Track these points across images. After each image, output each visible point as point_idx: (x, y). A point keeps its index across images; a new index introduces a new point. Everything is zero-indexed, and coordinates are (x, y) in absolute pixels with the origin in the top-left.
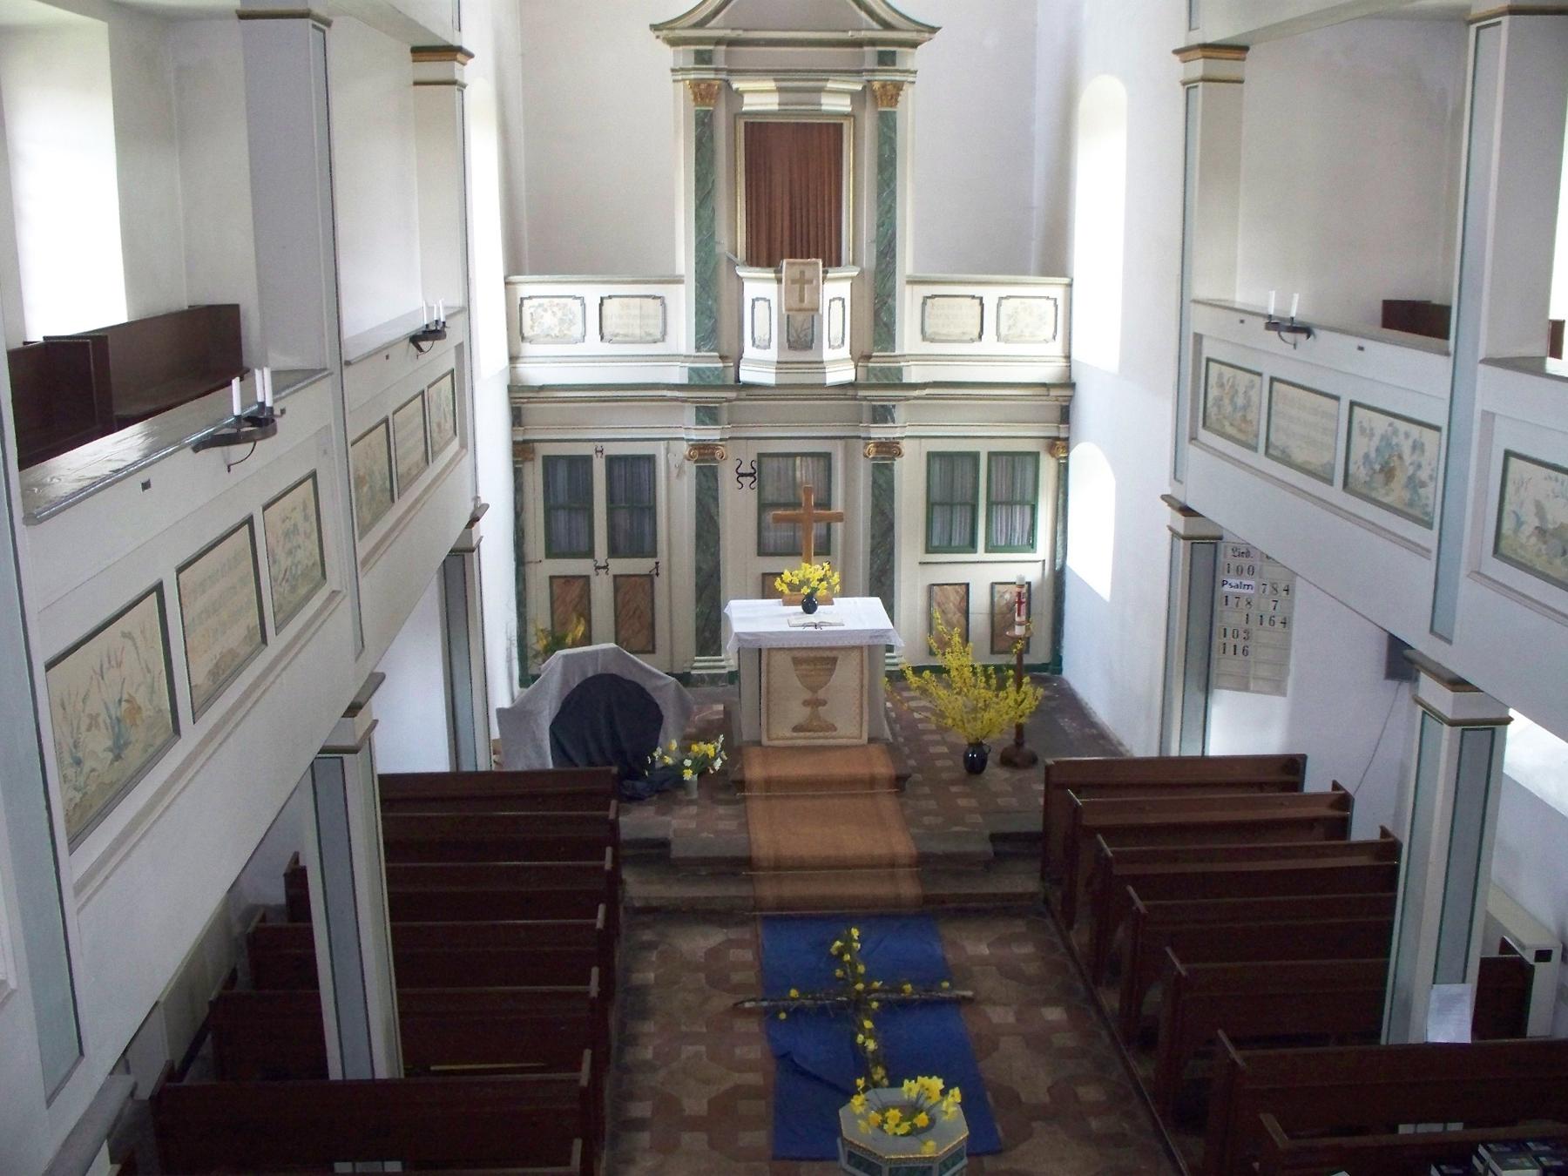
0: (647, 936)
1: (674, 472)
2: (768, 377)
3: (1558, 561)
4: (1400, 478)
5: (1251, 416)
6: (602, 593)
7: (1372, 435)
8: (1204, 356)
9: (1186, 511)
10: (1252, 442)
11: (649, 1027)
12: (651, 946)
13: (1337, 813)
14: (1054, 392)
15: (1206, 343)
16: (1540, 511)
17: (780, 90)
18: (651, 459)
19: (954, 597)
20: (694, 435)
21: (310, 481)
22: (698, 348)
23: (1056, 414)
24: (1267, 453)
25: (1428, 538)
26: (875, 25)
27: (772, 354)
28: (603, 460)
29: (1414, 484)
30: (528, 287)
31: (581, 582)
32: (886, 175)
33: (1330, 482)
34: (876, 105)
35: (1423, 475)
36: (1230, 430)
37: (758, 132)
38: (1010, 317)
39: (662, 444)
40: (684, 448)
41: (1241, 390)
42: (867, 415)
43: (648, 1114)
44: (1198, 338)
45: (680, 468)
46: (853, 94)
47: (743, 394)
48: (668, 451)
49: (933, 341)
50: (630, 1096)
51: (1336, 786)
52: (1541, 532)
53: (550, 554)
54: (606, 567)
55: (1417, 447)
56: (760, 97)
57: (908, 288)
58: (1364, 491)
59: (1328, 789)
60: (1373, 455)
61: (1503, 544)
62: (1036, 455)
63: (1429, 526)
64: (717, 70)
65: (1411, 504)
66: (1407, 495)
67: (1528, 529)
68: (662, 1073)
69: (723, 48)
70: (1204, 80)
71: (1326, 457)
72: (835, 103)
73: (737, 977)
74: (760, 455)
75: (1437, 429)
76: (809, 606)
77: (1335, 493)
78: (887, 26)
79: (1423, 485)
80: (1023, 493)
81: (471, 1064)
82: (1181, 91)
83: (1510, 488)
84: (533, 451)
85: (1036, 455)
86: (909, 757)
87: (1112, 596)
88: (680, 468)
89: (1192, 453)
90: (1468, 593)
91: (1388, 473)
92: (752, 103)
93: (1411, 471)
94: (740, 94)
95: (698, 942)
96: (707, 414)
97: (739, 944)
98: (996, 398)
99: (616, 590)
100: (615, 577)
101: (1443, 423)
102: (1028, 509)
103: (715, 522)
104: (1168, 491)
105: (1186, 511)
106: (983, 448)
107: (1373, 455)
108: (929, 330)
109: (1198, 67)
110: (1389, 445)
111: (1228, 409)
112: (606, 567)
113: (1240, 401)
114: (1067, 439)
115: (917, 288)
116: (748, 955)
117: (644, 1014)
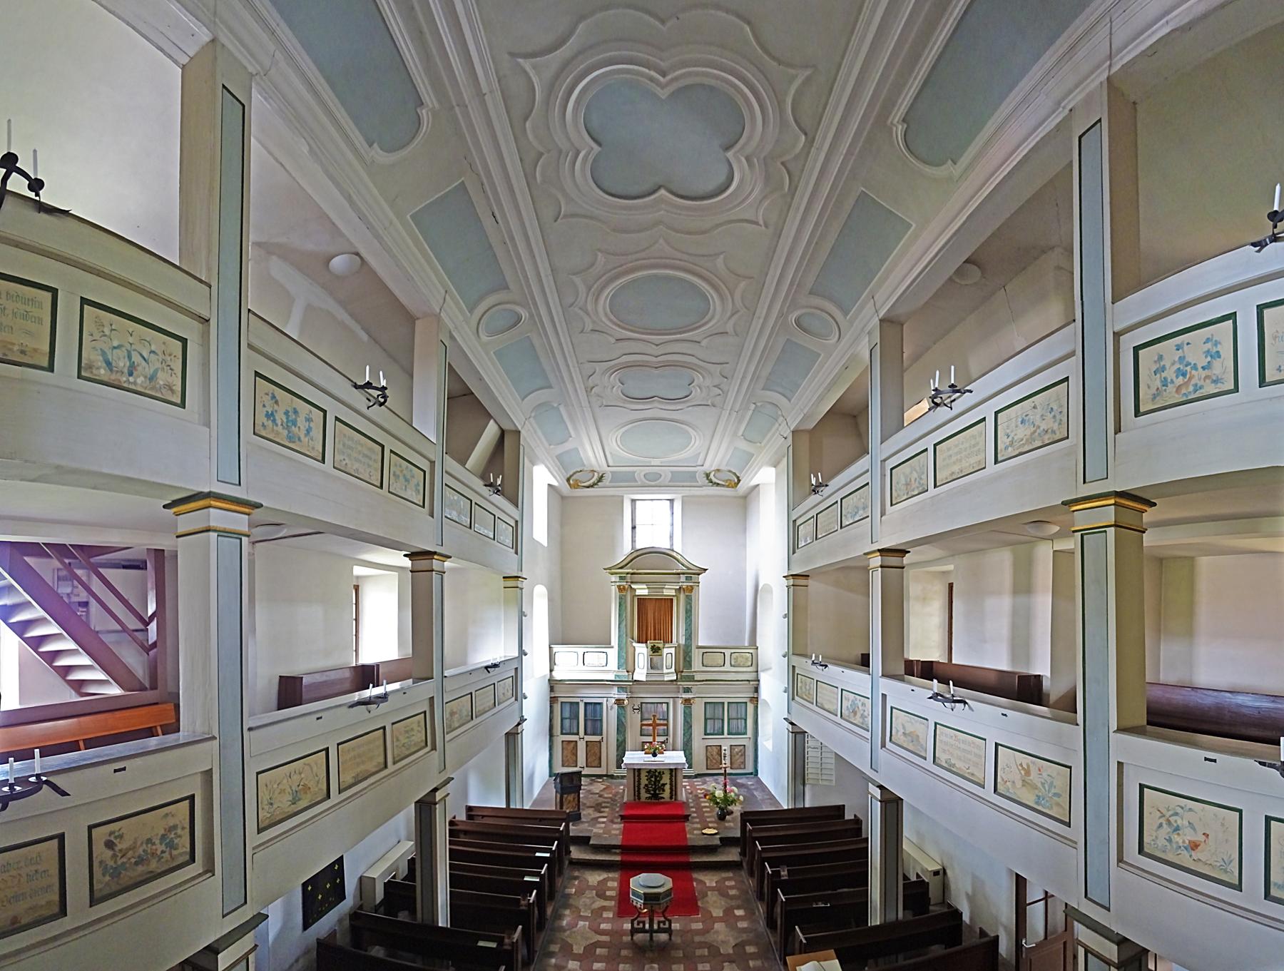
0: (576, 874)
1: (609, 708)
2: (644, 679)
3: (911, 744)
4: (859, 715)
5: (811, 693)
6: (582, 747)
7: (849, 700)
8: (796, 672)
9: (792, 724)
10: (811, 701)
11: (567, 912)
12: (576, 878)
13: (856, 826)
14: (751, 683)
15: (796, 669)
16: (904, 728)
17: (648, 588)
18: (600, 704)
19: (715, 750)
20: (616, 696)
21: (382, 730)
22: (619, 669)
23: (753, 690)
24: (816, 705)
25: (868, 735)
26: (684, 568)
27: (645, 671)
28: (583, 704)
29: (863, 716)
30: (556, 648)
31: (574, 743)
32: (688, 615)
33: (836, 715)
34: (684, 593)
35: (866, 714)
36: (805, 697)
37: (642, 601)
38: (735, 659)
39: (605, 699)
40: (613, 700)
41: (808, 684)
42: (681, 690)
43: (557, 950)
44: (794, 667)
45: (612, 708)
46: (676, 589)
47: (635, 683)
48: (607, 701)
49: (706, 666)
50: (552, 942)
51: (855, 816)
52: (904, 734)
53: (562, 734)
54: (583, 738)
55: (863, 704)
56: (642, 590)
57: (697, 650)
58: (847, 718)
59: (853, 818)
60: (849, 706)
61: (893, 738)
62: (746, 703)
63: (868, 731)
64: (627, 582)
65: (863, 723)
66: (861, 721)
67: (900, 733)
68: (568, 932)
69: (629, 575)
70: (793, 585)
71: (835, 707)
72: (669, 591)
73: (608, 893)
74: (642, 703)
75: (868, 698)
76: (655, 755)
77: (838, 719)
78: (689, 569)
79: (866, 717)
80: (741, 715)
81: (390, 961)
82: (786, 588)
83: (894, 719)
84: (557, 700)
85: (746, 703)
86: (692, 807)
87: (773, 749)
88: (612, 708)
89: (793, 703)
90: (882, 753)
91: (855, 713)
92: (638, 592)
93: (862, 712)
94: (635, 590)
95: (594, 878)
96: (621, 688)
97: (613, 880)
98: (731, 685)
99: (587, 746)
100: (587, 742)
101: (870, 697)
102: (743, 721)
103: (624, 725)
104: (786, 717)
105: (792, 724)
106: (726, 701)
107: (849, 706)
108: (705, 663)
109: (791, 582)
110: (854, 703)
111: (804, 690)
112: (583, 738)
113: (808, 687)
114: (757, 698)
115: (700, 650)
116: (615, 884)
117: (567, 906)
